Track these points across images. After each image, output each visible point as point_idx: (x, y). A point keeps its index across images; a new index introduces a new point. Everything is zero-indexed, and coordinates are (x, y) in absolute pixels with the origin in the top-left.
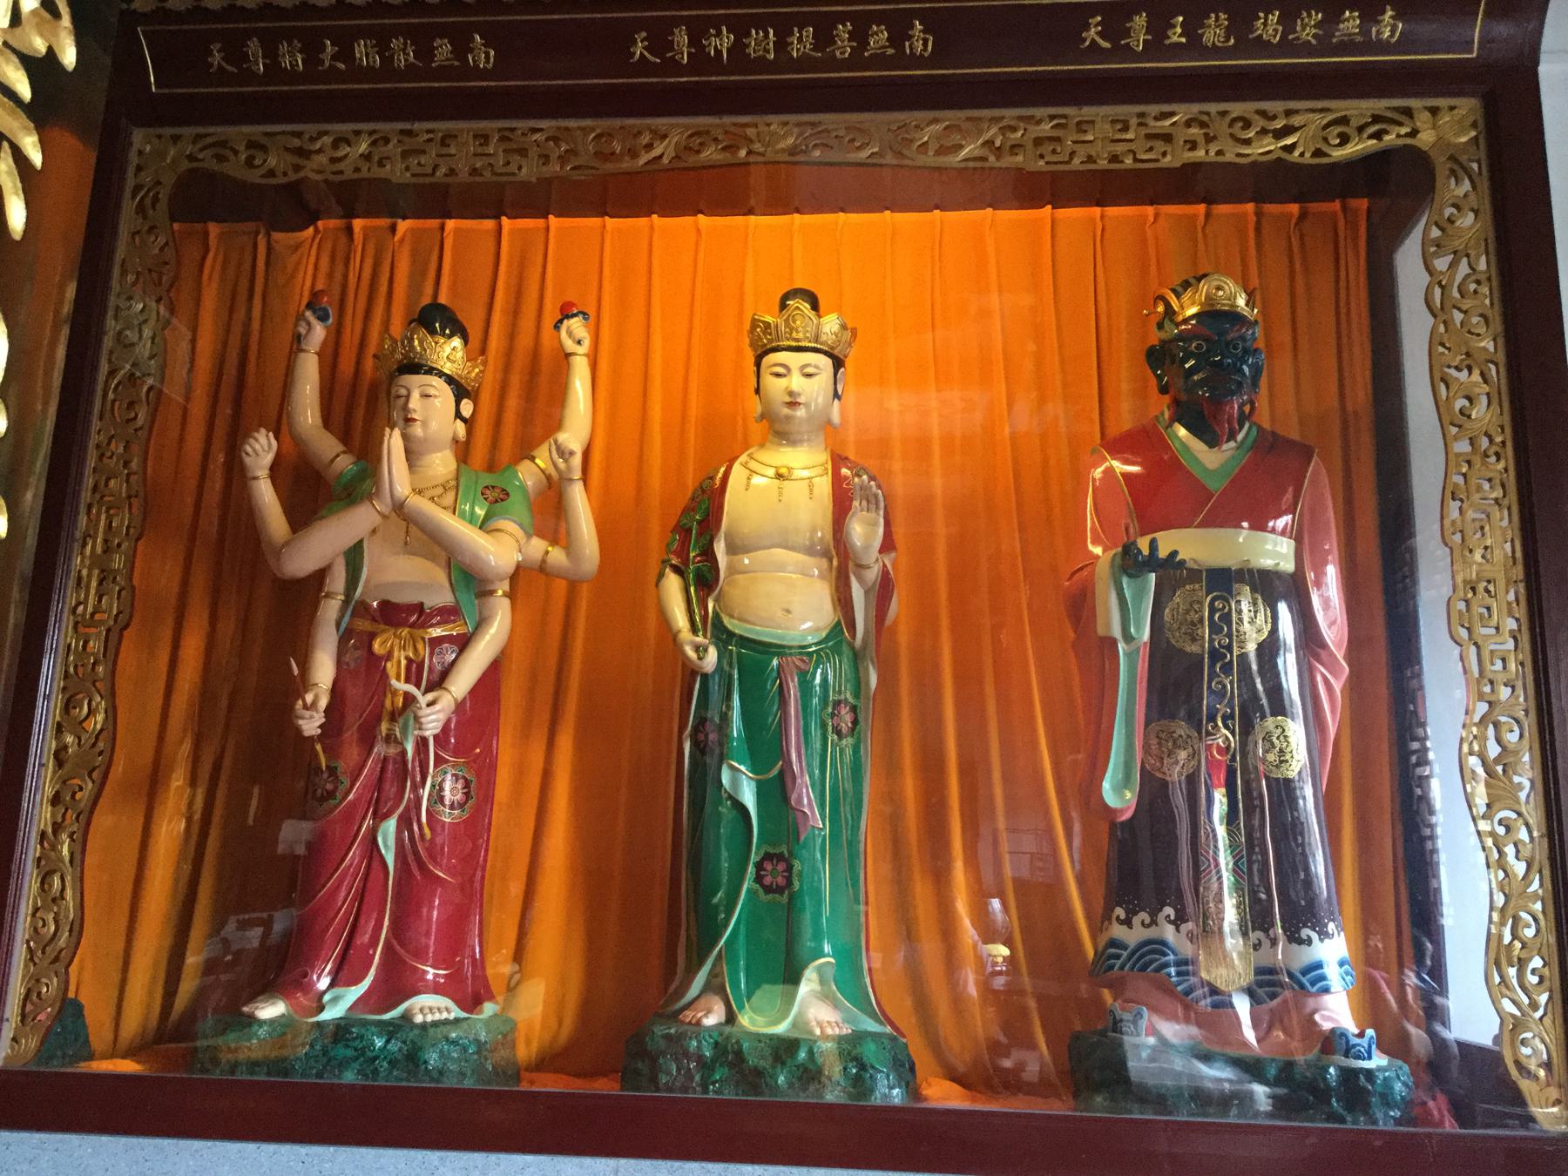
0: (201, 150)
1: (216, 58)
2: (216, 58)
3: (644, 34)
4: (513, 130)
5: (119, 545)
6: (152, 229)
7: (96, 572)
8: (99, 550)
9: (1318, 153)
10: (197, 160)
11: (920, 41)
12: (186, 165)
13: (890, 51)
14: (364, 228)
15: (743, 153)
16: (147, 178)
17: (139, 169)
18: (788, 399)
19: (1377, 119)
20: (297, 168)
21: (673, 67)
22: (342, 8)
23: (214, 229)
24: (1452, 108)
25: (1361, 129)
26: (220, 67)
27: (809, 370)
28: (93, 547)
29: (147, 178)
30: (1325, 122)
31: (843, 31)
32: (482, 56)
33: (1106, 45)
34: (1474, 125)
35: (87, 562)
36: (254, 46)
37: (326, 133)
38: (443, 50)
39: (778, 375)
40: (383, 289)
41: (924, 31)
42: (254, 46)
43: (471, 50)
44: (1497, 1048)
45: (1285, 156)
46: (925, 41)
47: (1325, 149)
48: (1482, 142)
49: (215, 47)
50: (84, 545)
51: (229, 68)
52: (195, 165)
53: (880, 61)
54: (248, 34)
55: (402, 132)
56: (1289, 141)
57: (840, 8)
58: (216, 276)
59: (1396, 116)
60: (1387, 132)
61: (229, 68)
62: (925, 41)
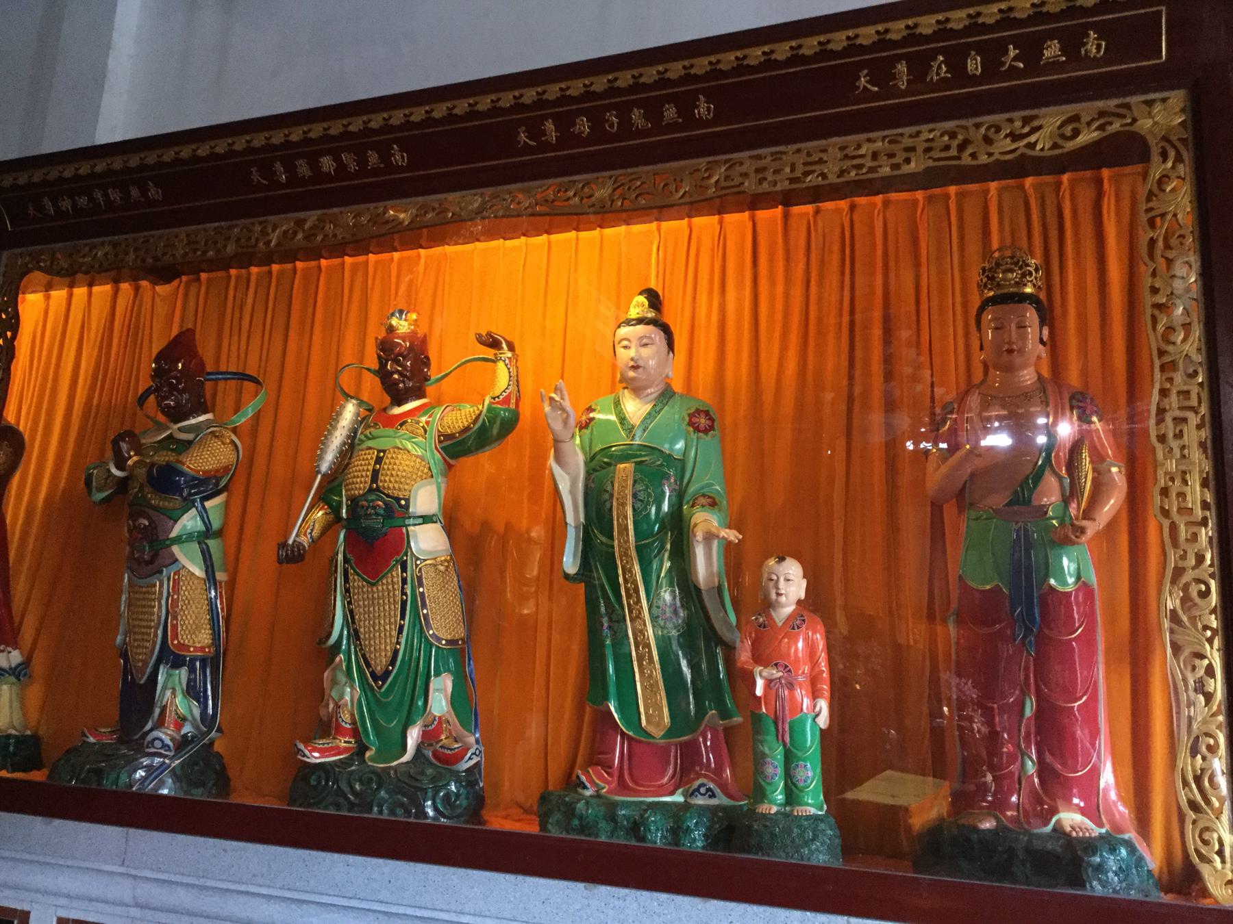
3: (866, 71)
4: (902, 135)
9: (1055, 146)
11: (1093, 46)
14: (1035, 187)
15: (319, 238)
18: (632, 363)
19: (1102, 114)
21: (545, 146)
22: (1038, 16)
23: (1106, 173)
24: (1164, 100)
25: (1089, 124)
26: (865, 87)
30: (1058, 123)
34: (1183, 111)
36: (278, 167)
37: (236, 226)
38: (135, 193)
39: (625, 347)
41: (707, 102)
42: (278, 167)
45: (1029, 152)
47: (1060, 142)
48: (1189, 124)
51: (531, 143)
53: (376, 172)
54: (544, 118)
55: (751, 157)
56: (1033, 139)
57: (683, 89)
58: (1113, 214)
59: (1121, 111)
60: (1111, 123)
61: (531, 143)
62: (403, 157)
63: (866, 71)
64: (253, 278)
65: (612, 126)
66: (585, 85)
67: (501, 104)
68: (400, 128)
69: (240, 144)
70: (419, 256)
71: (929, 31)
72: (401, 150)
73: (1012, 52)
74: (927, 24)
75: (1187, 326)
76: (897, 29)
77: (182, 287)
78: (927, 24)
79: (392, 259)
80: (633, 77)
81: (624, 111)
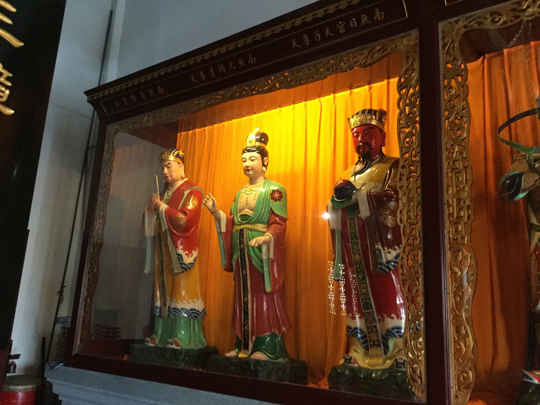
0: (469, 23)
1: (294, 44)
2: (294, 44)
3: (328, 28)
5: (463, 188)
6: (454, 59)
7: (455, 200)
8: (455, 191)
10: (469, 27)
12: (464, 30)
13: (369, 22)
16: (448, 39)
17: (443, 38)
20: (517, 17)
27: (253, 158)
28: (453, 190)
29: (448, 39)
31: (305, 37)
32: (379, 15)
33: (299, 46)
35: (451, 196)
40: (486, 82)
43: (249, 59)
44: (151, 337)
46: (381, 15)
49: (159, 87)
50: (448, 190)
51: (299, 46)
52: (469, 29)
53: (366, 26)
63: (328, 28)
64: (182, 136)
65: (318, 38)
66: (244, 42)
67: (307, 20)
68: (322, 19)
69: (184, 64)
70: (252, 119)
71: (344, 7)
72: (161, 87)
73: (231, 64)
74: (331, 9)
75: (448, 186)
76: (320, 13)
77: (486, 61)
78: (331, 9)
79: (214, 128)
80: (244, 42)
81: (322, 29)
